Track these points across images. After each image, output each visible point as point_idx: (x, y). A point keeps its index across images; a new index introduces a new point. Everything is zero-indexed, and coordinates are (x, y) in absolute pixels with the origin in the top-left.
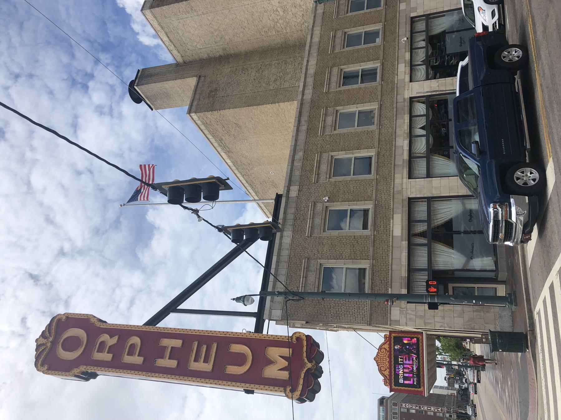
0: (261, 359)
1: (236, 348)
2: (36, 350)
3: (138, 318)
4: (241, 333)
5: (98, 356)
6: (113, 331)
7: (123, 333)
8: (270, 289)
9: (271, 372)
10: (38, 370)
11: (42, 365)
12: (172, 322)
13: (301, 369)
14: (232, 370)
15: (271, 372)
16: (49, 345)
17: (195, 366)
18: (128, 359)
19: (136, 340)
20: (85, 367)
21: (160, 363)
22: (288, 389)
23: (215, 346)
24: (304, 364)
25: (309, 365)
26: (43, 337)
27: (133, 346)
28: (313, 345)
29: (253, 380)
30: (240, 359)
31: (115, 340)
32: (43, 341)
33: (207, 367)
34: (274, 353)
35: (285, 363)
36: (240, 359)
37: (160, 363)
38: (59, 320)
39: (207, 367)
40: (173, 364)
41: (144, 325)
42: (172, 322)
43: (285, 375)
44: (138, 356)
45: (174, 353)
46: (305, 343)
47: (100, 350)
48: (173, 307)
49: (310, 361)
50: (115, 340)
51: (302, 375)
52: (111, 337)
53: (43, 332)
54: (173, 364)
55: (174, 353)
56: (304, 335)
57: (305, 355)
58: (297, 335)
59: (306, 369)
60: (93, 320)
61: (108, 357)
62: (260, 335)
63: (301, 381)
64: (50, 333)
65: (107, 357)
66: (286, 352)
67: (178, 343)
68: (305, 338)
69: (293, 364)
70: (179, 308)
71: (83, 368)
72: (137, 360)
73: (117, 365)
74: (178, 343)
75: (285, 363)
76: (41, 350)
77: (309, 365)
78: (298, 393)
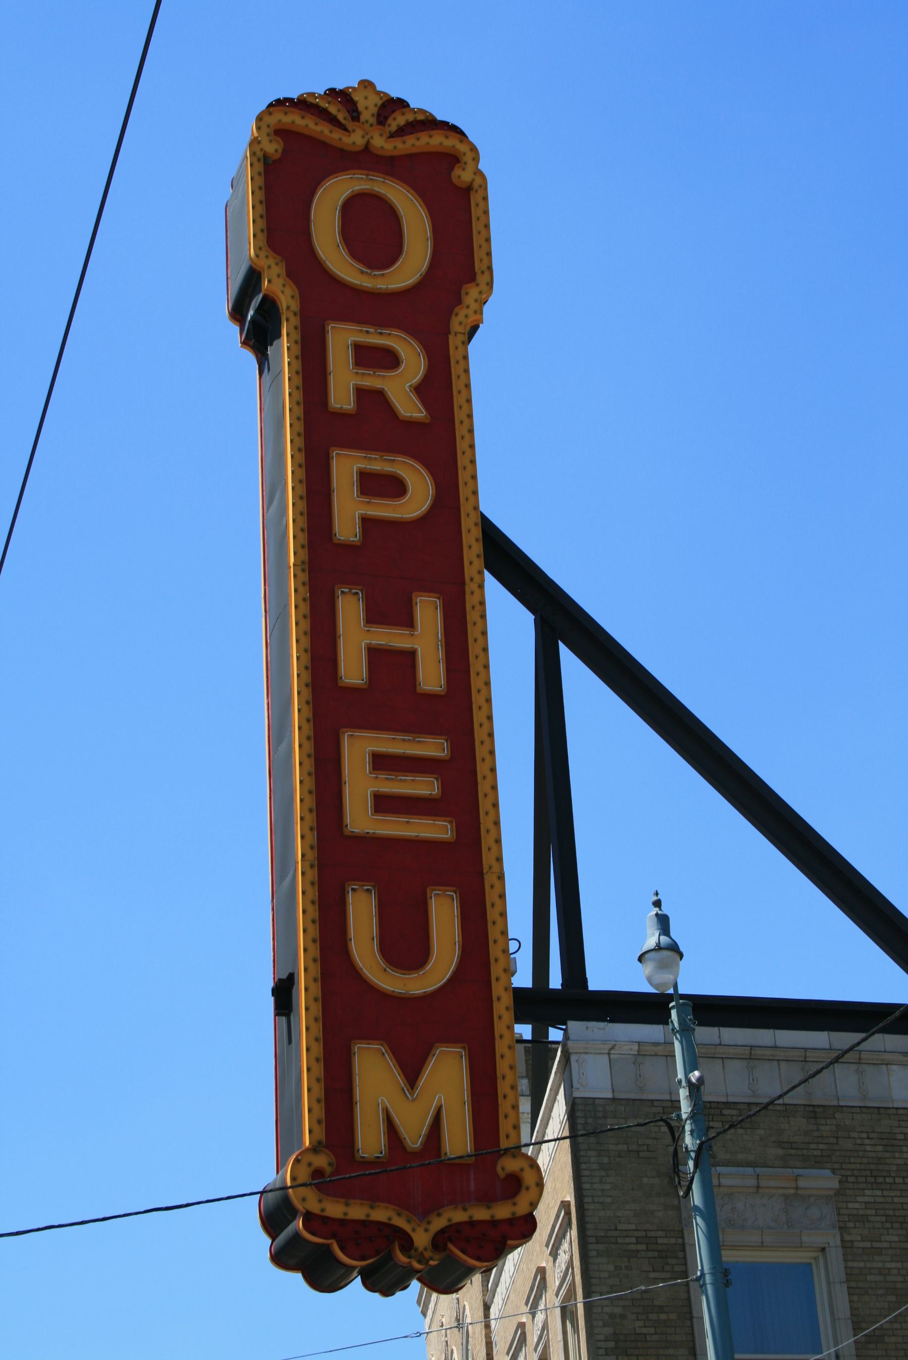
0: (411, 1034)
1: (444, 915)
2: (332, 93)
3: (509, 491)
4: (505, 933)
5: (341, 340)
6: (444, 388)
7: (441, 436)
8: (831, 1280)
9: (374, 1072)
10: (259, 119)
11: (281, 133)
12: (508, 627)
13: (403, 1204)
14: (362, 912)
15: (374, 1072)
16: (355, 139)
17: (357, 749)
18: (345, 467)
19: (418, 498)
20: (295, 306)
21: (350, 609)
22: (322, 1161)
23: (437, 830)
24: (424, 1211)
25: (421, 1239)
26: (383, 106)
27: (394, 487)
28: (492, 1242)
29: (338, 1013)
30: (405, 943)
31: (409, 407)
32: (368, 106)
33: (359, 818)
34: (447, 1075)
35: (414, 1135)
36: (405, 943)
37: (350, 609)
38: (452, 159)
39: (359, 818)
40: (353, 669)
41: (483, 516)
42: (508, 627)
43: (369, 1141)
44: (366, 521)
45: (393, 666)
46: (502, 1212)
47: (366, 357)
48: (561, 622)
49: (439, 1241)
50: (409, 407)
51: (381, 1214)
52: (419, 390)
53: (401, 104)
54: (353, 669)
55: (393, 666)
56: (534, 1205)
57: (459, 1216)
58: (529, 1178)
59: (407, 1227)
60: (471, 294)
61: (341, 394)
62: (508, 1016)
63: (357, 1212)
64: (402, 132)
65: (343, 387)
66: (458, 1140)
67: (431, 676)
68: (521, 1209)
69: (416, 1170)
70: (564, 651)
71: (287, 299)
72: (349, 514)
73: (320, 431)
74: (431, 676)
75: (414, 1135)
76: (333, 109)
77: (421, 1239)
78: (312, 1201)
